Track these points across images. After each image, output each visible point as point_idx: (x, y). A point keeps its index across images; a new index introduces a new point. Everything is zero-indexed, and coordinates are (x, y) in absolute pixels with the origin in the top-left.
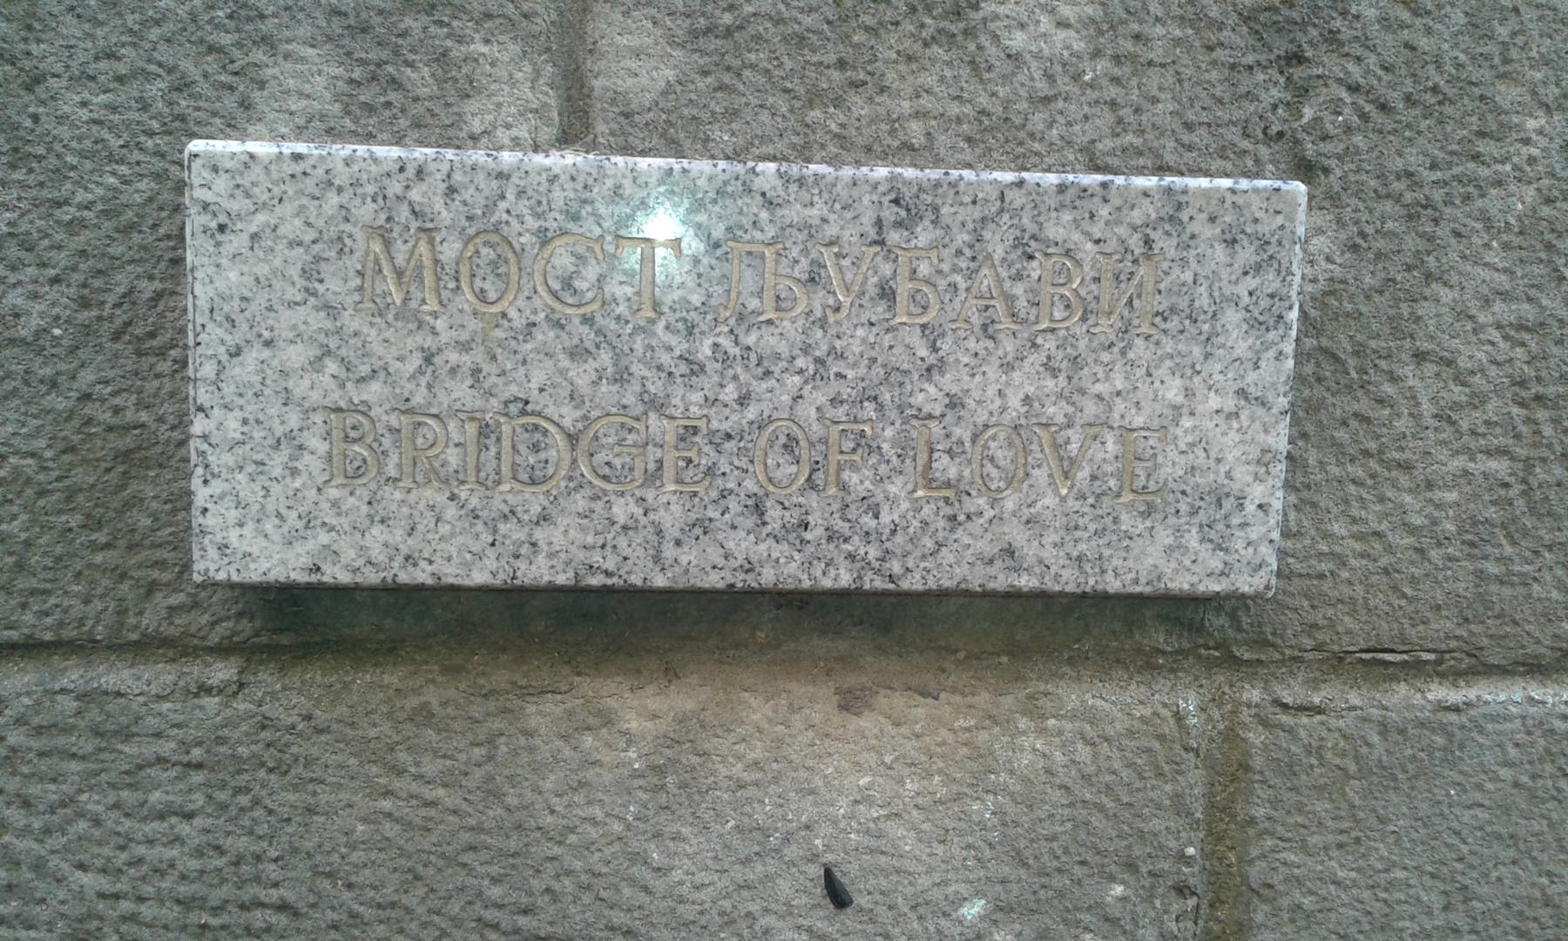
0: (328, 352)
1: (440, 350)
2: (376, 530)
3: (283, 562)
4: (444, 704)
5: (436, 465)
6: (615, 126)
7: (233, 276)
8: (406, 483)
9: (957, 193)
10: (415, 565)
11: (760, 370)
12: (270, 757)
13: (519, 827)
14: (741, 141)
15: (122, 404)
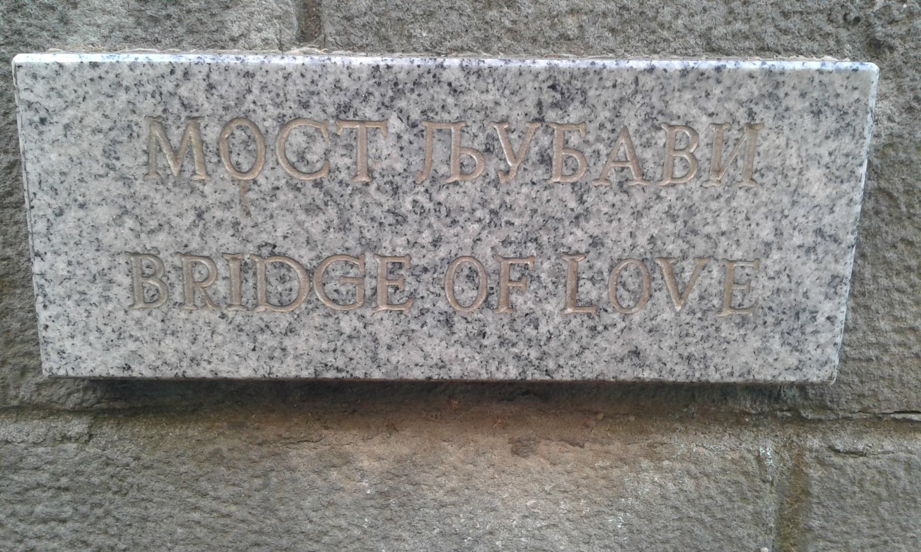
0: (126, 212)
1: (208, 209)
2: (169, 340)
3: (104, 363)
4: (231, 450)
5: (210, 292)
6: (340, 28)
7: (54, 156)
8: (189, 307)
10: (198, 365)
11: (449, 220)
12: (114, 484)
13: (288, 531)
14: (436, 37)
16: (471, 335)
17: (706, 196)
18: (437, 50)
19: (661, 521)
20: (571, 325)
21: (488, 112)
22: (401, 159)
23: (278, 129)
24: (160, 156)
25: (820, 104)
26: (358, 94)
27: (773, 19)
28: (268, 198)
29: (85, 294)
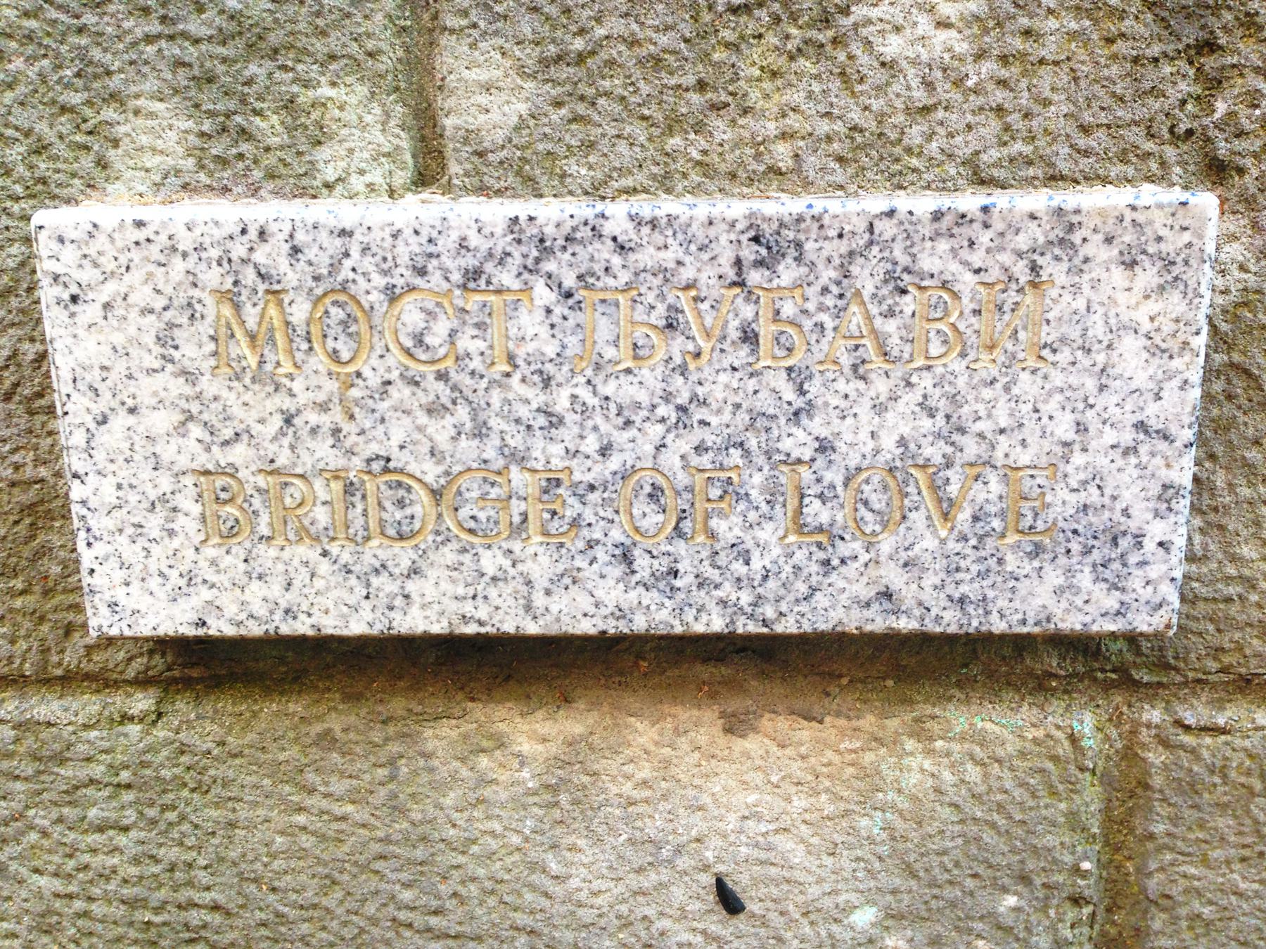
0: (191, 418)
1: (299, 411)
2: (255, 585)
4: (345, 730)
5: (306, 522)
6: (469, 166)
8: (280, 541)
9: (822, 227)
10: (295, 618)
11: (620, 420)
13: (424, 839)
15: (21, 461)
16: (657, 574)
17: (975, 381)
18: (601, 192)
19: (936, 824)
20: (794, 558)
21: (668, 275)
22: (553, 340)
23: (386, 304)
24: (232, 343)
25: (1134, 252)
26: (491, 255)
27: (1068, 136)
28: (377, 396)
29: (141, 527)
